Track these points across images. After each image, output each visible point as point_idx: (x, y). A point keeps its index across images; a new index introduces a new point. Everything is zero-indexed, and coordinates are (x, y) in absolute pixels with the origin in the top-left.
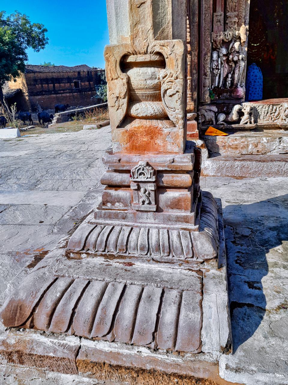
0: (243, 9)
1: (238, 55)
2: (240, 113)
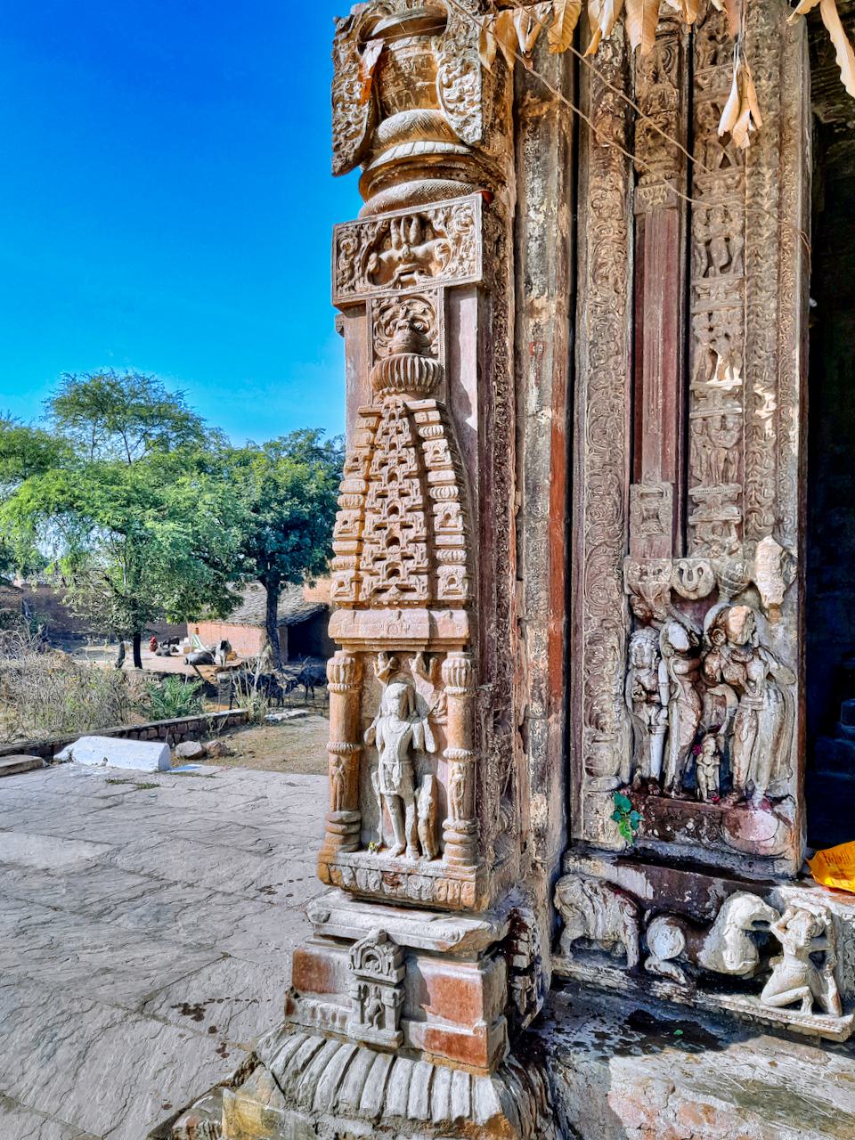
0: (765, 471)
2: (766, 946)
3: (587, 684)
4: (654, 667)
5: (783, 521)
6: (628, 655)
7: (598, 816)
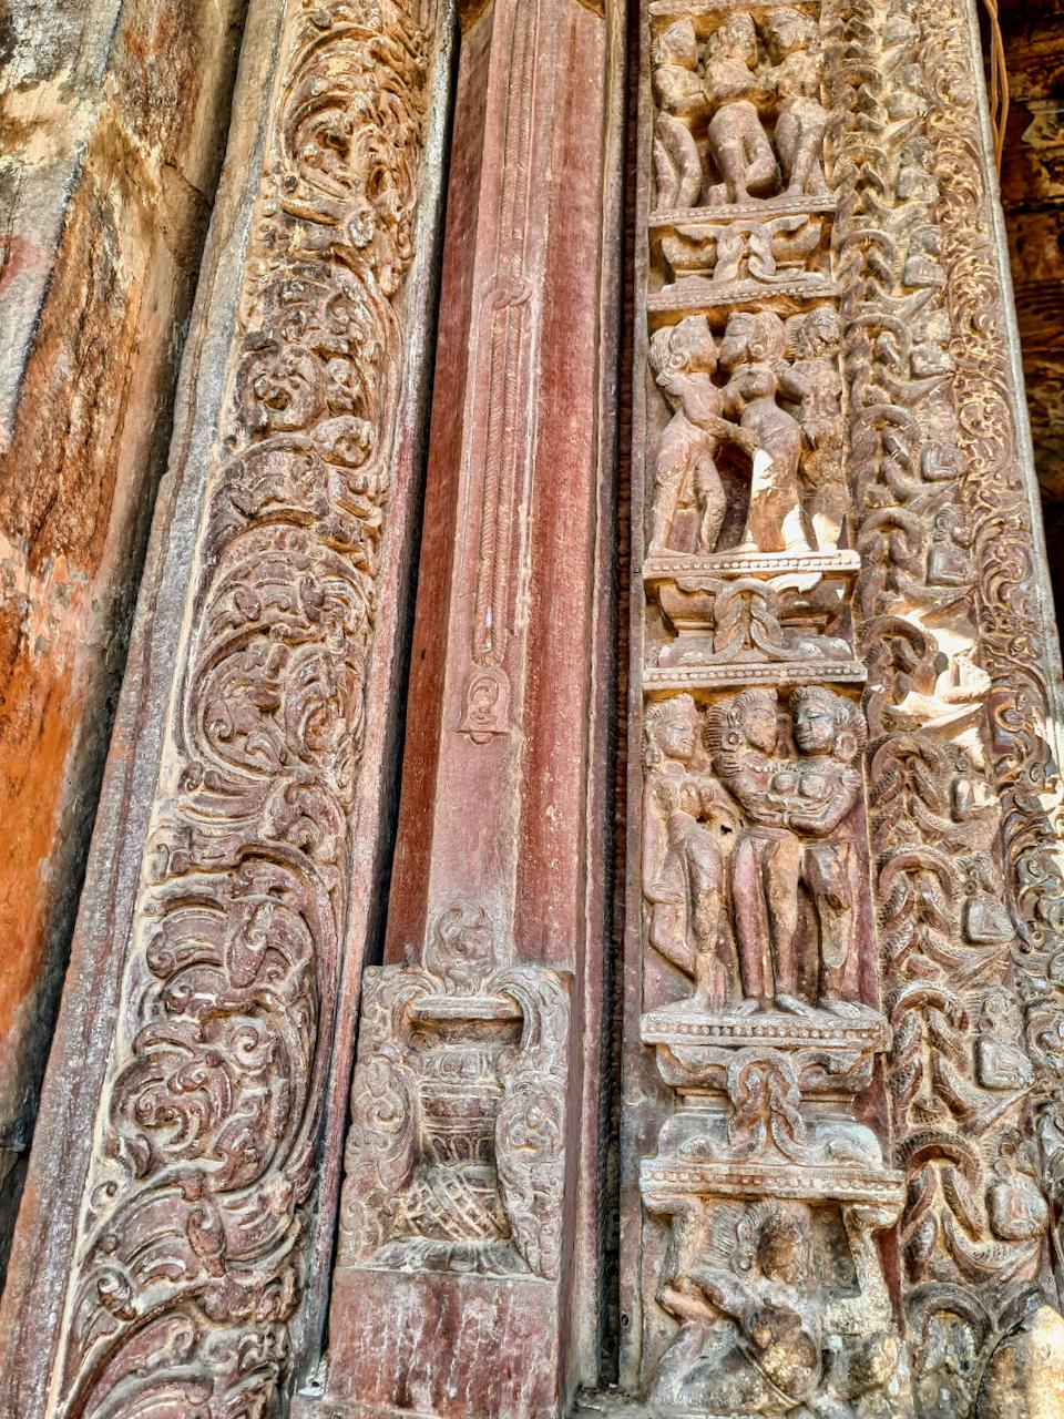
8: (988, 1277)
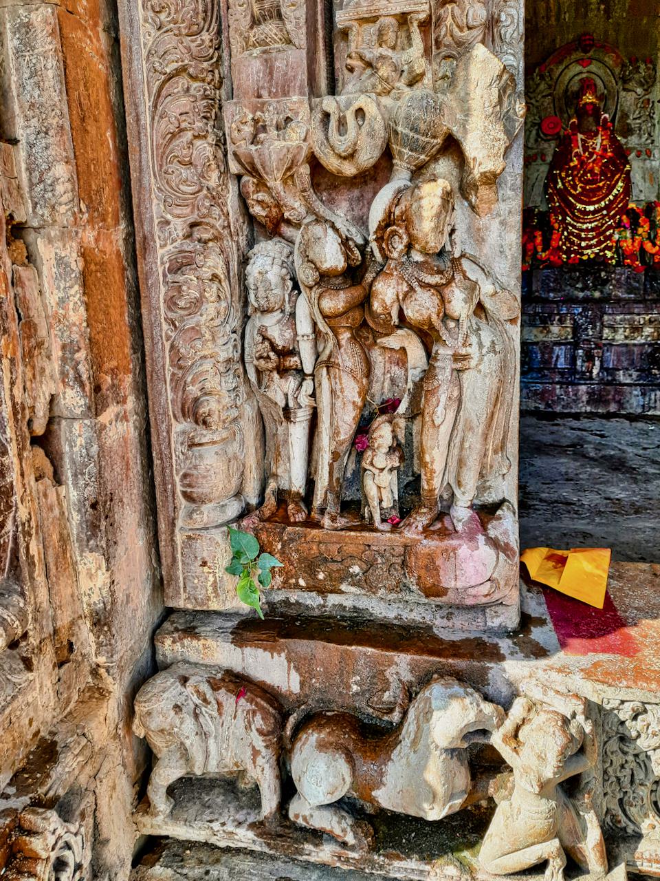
1: (434, 279)
2: (482, 762)
3: (172, 347)
4: (288, 309)
5: (498, 21)
6: (245, 290)
7: (206, 569)
8: (464, 43)
